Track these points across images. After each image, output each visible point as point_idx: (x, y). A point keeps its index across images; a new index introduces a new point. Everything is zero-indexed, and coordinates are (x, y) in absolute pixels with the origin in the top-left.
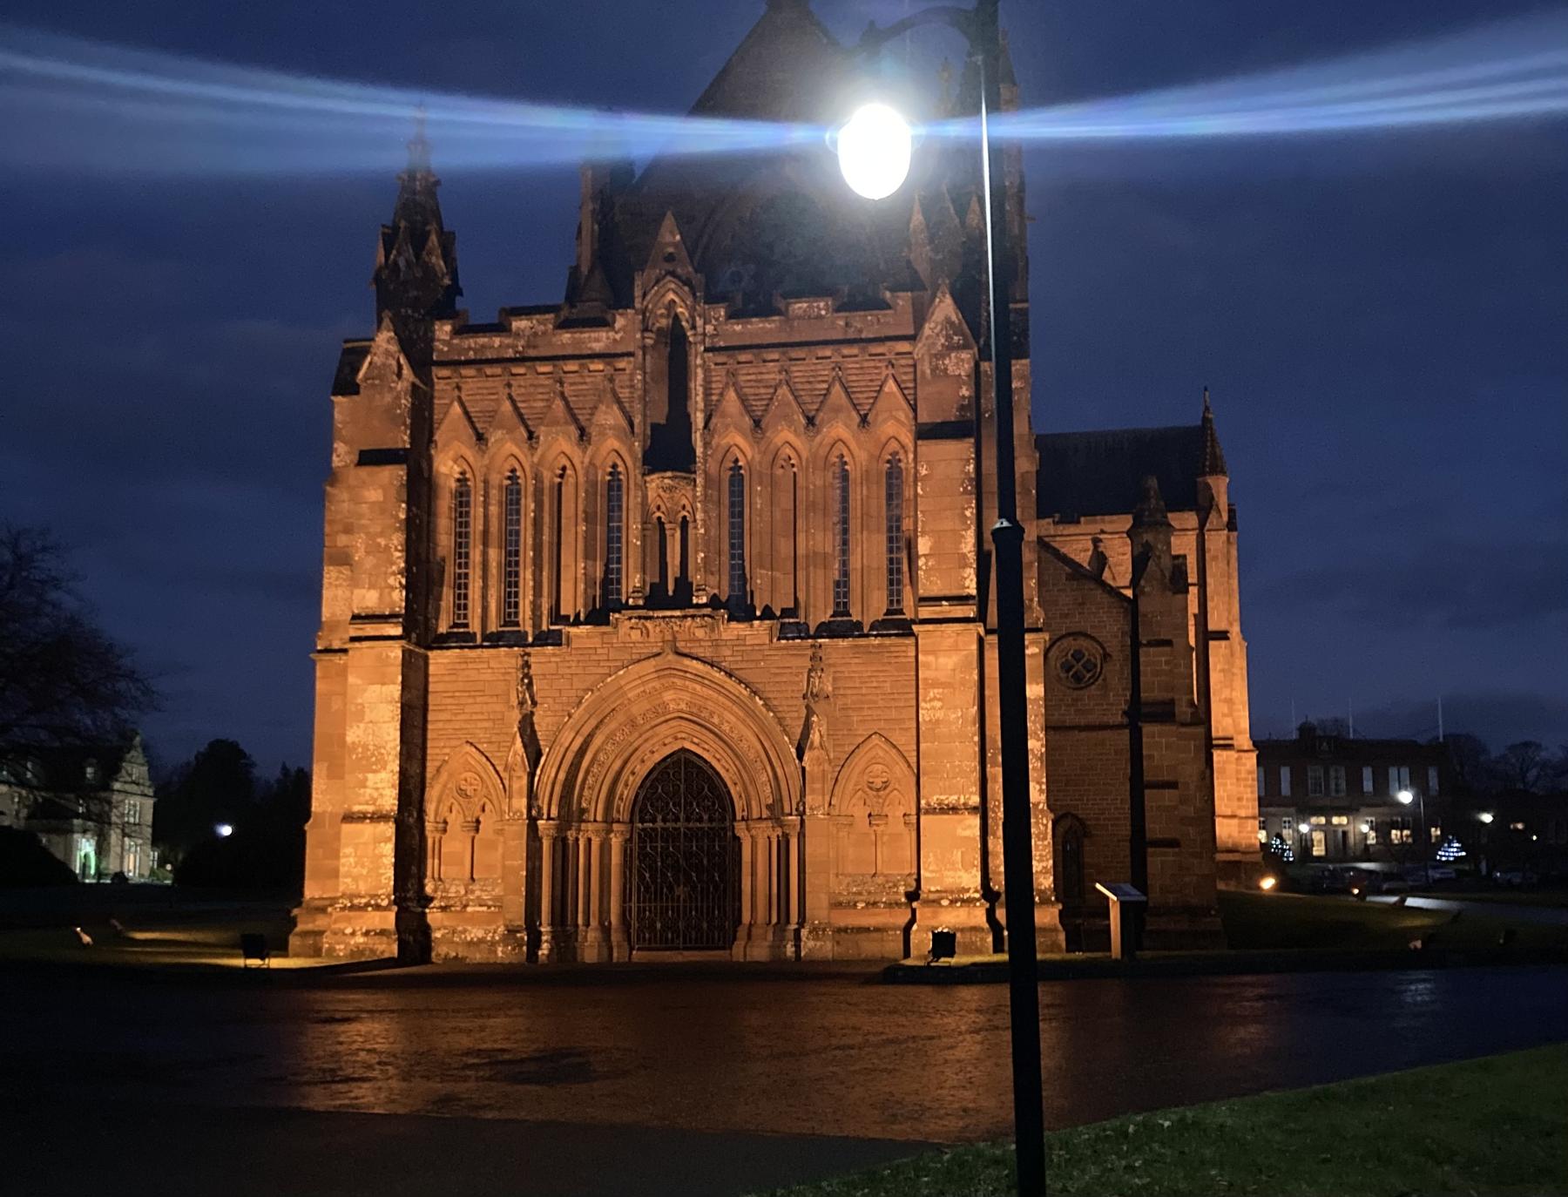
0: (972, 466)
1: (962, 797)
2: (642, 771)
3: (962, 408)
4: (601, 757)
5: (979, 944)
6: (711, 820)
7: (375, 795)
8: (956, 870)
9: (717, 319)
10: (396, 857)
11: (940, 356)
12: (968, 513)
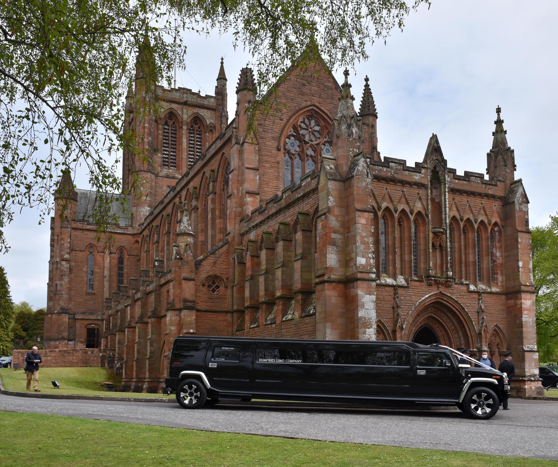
7: (369, 337)
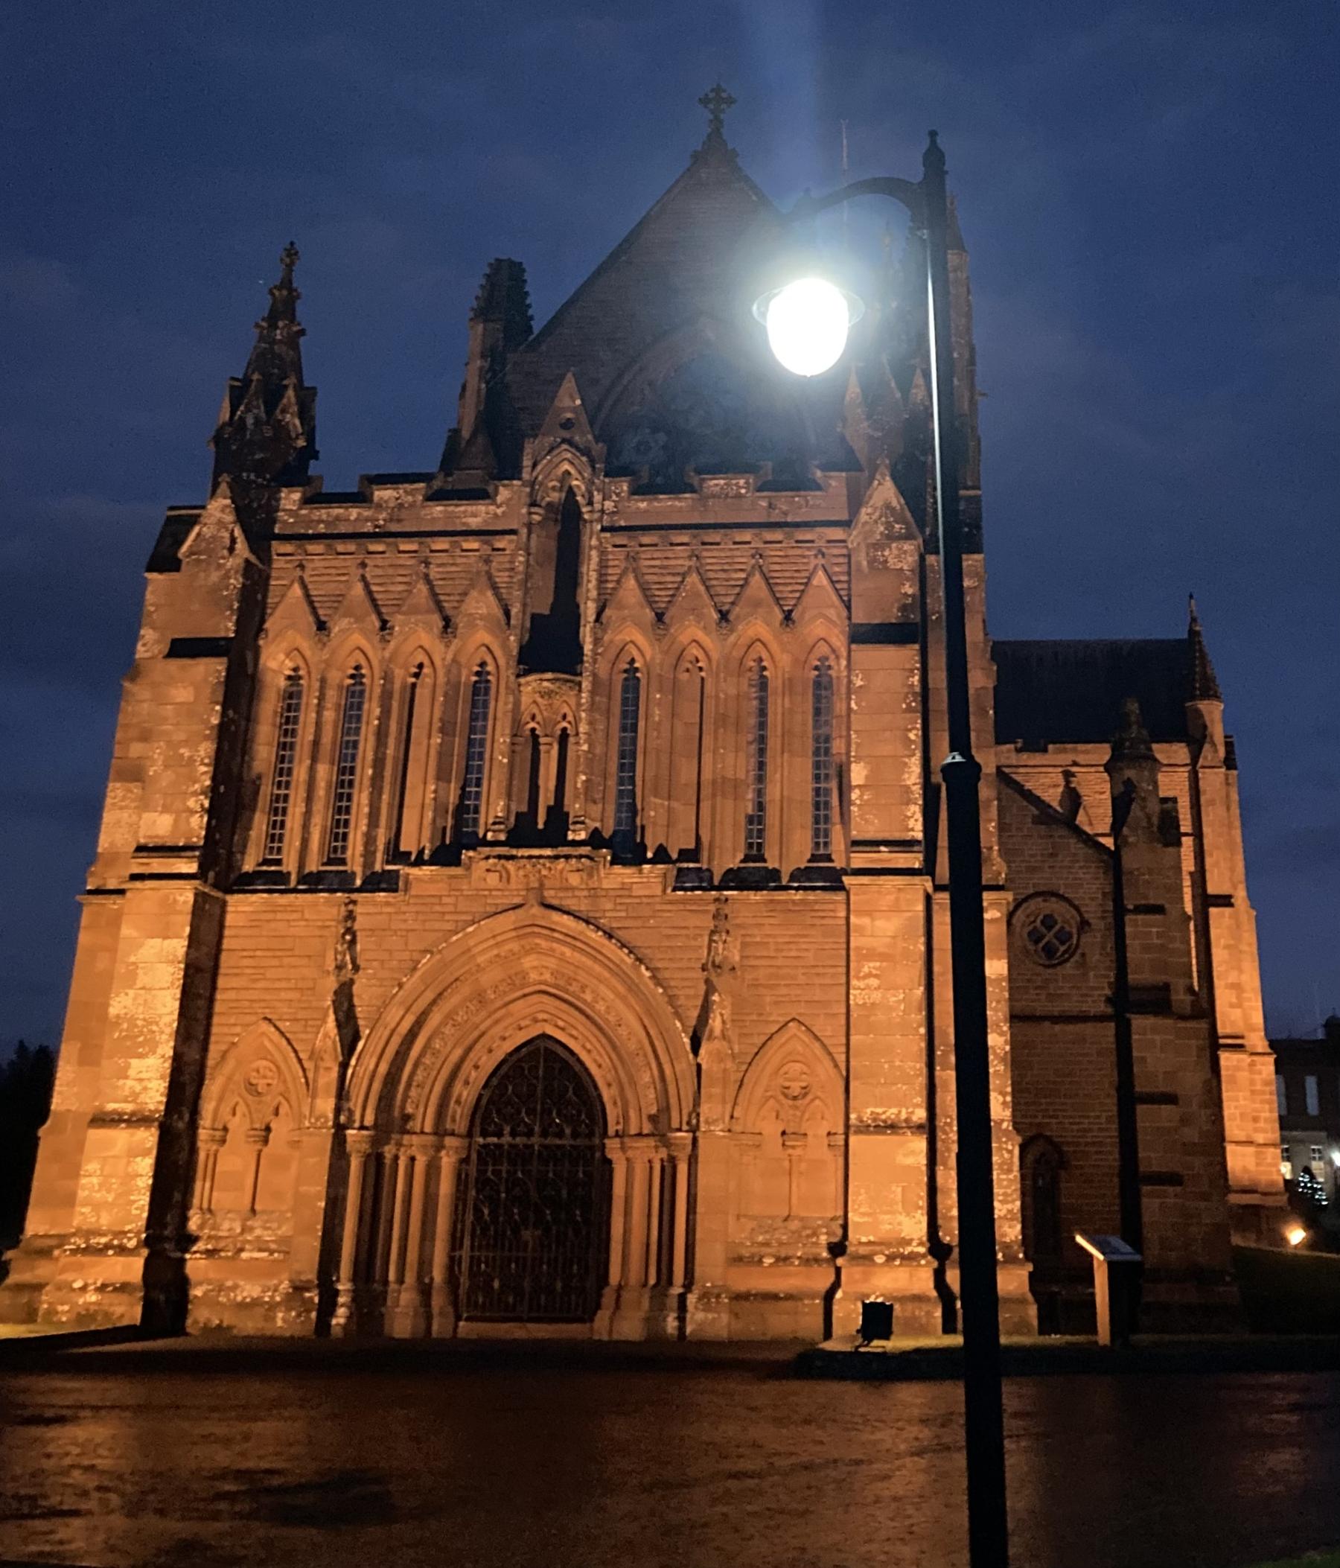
0: (917, 678)
4: (437, 1044)
9: (618, 495)
12: (912, 736)
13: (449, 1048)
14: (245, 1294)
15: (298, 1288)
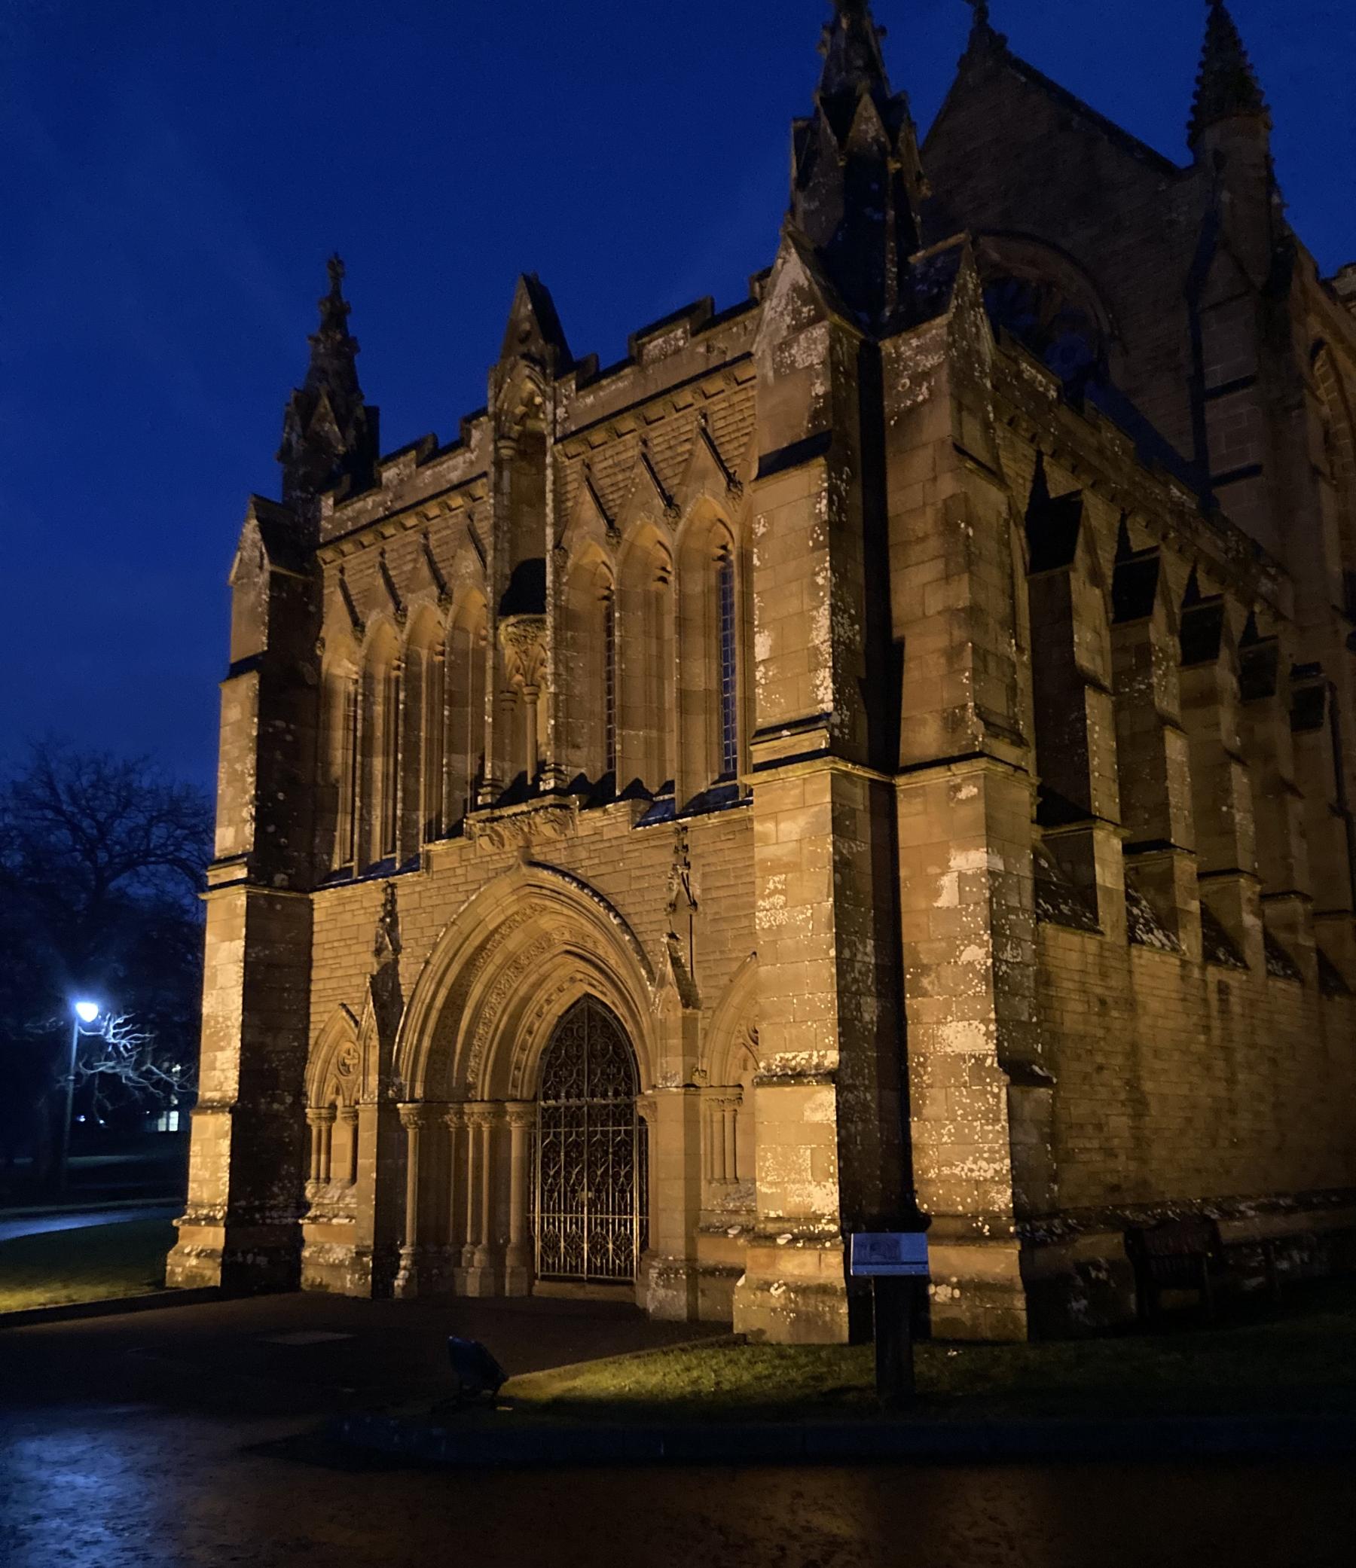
0: (825, 502)
1: (815, 1053)
2: (544, 1028)
3: (816, 415)
4: (487, 1012)
5: (828, 1317)
6: (616, 1094)
8: (802, 1182)
9: (567, 397)
10: (232, 1156)
11: (785, 345)
12: (820, 581)
13: (498, 1015)
14: (335, 1256)
15: (360, 1254)
